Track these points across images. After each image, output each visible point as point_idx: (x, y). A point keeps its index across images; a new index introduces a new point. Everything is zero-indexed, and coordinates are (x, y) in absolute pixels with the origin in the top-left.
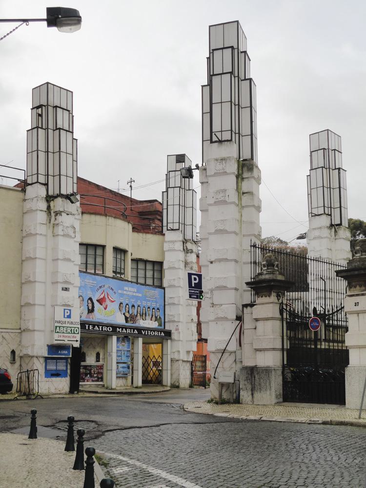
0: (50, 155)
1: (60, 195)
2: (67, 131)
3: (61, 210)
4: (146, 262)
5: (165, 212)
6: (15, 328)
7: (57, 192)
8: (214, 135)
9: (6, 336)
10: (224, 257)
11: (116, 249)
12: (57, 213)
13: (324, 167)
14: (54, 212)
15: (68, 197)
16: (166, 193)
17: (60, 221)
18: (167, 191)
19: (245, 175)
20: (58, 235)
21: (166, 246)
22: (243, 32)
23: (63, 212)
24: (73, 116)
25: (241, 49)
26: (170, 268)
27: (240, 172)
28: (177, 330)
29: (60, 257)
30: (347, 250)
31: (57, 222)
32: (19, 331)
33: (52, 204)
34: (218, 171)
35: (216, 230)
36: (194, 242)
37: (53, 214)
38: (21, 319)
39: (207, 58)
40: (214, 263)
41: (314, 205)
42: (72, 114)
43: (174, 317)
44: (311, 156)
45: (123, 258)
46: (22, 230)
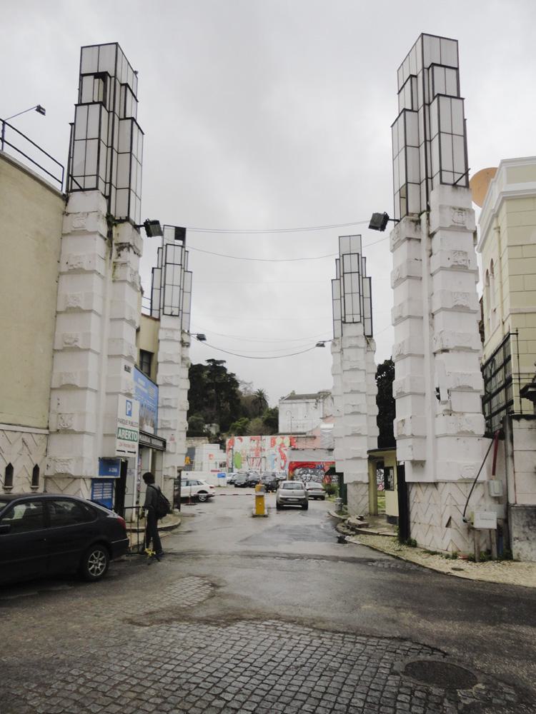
6: (41, 426)
9: (28, 439)
10: (468, 345)
12: (122, 247)
14: (116, 244)
21: (162, 335)
25: (363, 256)
28: (172, 439)
32: (47, 432)
34: (456, 224)
37: (115, 248)
38: (49, 411)
40: (450, 351)
41: (349, 311)
43: (170, 424)
46: (59, 262)
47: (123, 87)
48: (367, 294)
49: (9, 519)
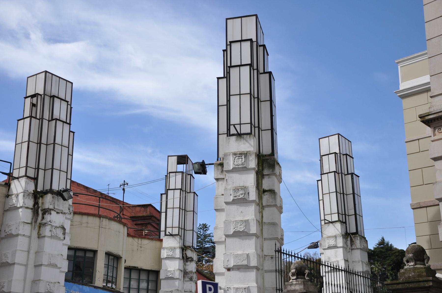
0: (43, 147)
1: (51, 191)
2: (63, 122)
3: (51, 207)
4: (139, 270)
5: (163, 215)
7: (48, 187)
8: (232, 127)
11: (108, 254)
12: (46, 211)
13: (336, 172)
15: (60, 194)
16: (165, 195)
17: (48, 220)
18: (166, 194)
19: (266, 172)
20: (44, 237)
21: (164, 254)
22: (261, 27)
23: (53, 210)
24: (71, 108)
25: (261, 43)
26: (168, 278)
27: (261, 168)
29: (45, 262)
30: (366, 262)
31: (44, 221)
33: (40, 201)
34: (237, 166)
35: (234, 232)
36: (195, 249)
37: (40, 213)
39: (224, 51)
40: (231, 270)
41: (234, 120)
42: (71, 105)
44: (321, 160)
45: (115, 266)
47: (345, 156)
48: (265, 95)
49: (74, 276)
